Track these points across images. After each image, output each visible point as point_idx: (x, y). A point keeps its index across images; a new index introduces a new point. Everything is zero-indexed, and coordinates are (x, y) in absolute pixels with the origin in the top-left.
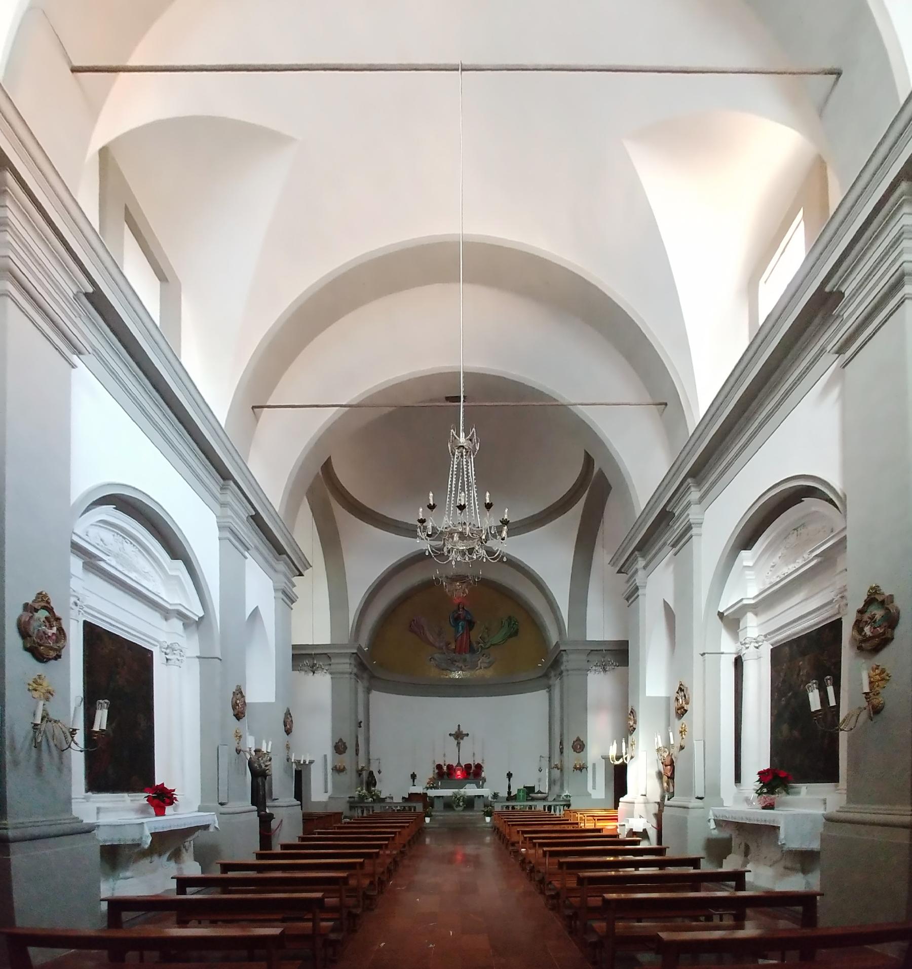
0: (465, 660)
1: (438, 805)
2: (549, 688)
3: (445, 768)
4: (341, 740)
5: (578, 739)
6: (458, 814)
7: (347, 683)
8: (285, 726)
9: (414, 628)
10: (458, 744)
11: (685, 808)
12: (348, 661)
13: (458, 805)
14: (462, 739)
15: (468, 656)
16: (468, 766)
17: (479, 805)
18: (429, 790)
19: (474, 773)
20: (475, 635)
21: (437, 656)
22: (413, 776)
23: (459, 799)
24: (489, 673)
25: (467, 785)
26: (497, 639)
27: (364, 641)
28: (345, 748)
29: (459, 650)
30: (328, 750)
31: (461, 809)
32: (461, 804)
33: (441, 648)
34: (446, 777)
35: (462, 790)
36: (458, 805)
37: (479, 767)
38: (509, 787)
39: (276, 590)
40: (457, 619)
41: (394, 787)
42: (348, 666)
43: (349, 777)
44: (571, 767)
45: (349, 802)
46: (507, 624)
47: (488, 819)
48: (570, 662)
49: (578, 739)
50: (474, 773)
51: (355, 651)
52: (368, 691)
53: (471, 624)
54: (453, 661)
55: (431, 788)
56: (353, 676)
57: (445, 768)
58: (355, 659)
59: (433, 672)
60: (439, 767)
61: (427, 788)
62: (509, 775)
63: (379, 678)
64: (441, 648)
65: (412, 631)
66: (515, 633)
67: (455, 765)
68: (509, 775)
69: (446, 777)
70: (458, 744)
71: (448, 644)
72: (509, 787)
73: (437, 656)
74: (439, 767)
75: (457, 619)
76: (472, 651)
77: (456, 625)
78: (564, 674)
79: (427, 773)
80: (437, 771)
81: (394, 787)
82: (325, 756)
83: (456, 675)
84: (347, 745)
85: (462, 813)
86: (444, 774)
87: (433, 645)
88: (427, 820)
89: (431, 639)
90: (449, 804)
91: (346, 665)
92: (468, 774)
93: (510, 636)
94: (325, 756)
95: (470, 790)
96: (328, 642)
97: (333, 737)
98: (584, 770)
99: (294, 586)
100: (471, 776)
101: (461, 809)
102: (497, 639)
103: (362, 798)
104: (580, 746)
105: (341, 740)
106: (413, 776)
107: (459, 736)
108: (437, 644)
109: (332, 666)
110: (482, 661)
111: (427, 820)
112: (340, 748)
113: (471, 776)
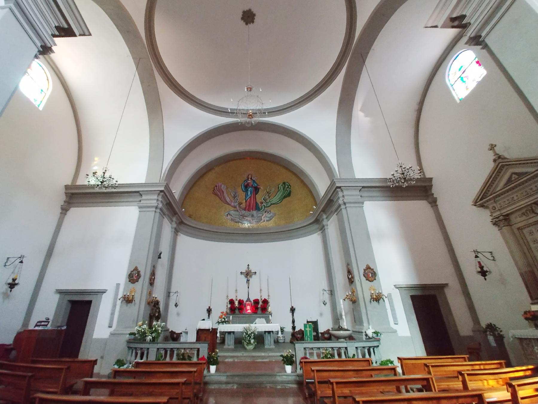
0: (253, 216)
1: (230, 342)
2: (322, 229)
3: (236, 303)
4: (136, 269)
5: (368, 268)
6: (249, 354)
7: (151, 216)
8: (150, 280)
9: (217, 192)
10: (248, 281)
11: (359, 332)
12: (155, 197)
13: (249, 343)
14: (251, 276)
15: (255, 213)
16: (256, 302)
17: (269, 341)
18: (221, 325)
19: (261, 308)
20: (260, 198)
21: (232, 212)
22: (209, 311)
23: (249, 336)
24: (271, 224)
25: (258, 320)
26: (275, 200)
27: (177, 190)
28: (139, 276)
29: (248, 208)
30: (122, 278)
31: (251, 347)
32: (252, 341)
33: (235, 207)
34: (237, 311)
35: (253, 326)
36: (249, 343)
37: (266, 302)
38: (293, 322)
39: (172, 228)
40: (246, 187)
41: (187, 320)
42: (155, 201)
43: (140, 308)
44: (368, 298)
45: (129, 342)
46: (282, 188)
47: (289, 369)
48: (347, 196)
49: (368, 268)
50: (261, 308)
51: (162, 189)
52: (176, 232)
53: (256, 190)
54: (244, 216)
55: (223, 322)
56: (158, 211)
57: (236, 303)
58: (163, 197)
59: (230, 224)
60: (232, 302)
61: (219, 323)
62: (293, 310)
63: (186, 224)
64: (235, 207)
65: (216, 195)
66: (289, 195)
67: (245, 300)
68: (293, 310)
69: (237, 311)
70: (248, 281)
71: (240, 204)
72: (293, 322)
73: (232, 212)
74: (232, 302)
75: (246, 187)
76: (257, 208)
77: (246, 191)
78: (343, 207)
79: (221, 307)
80: (229, 306)
81: (187, 320)
82: (118, 285)
83: (246, 225)
84: (142, 273)
85: (254, 354)
86: (236, 309)
87: (228, 204)
88: (213, 368)
89: (228, 200)
90: (240, 341)
91: (153, 200)
92: (257, 308)
93: (285, 197)
94: (118, 285)
95: (260, 325)
96: (144, 182)
97: (129, 266)
98: (381, 301)
99: (55, 45)
100: (259, 311)
101: (251, 347)
102: (275, 200)
103: (143, 334)
104: (371, 274)
105: (136, 269)
106: (209, 311)
107: (248, 274)
108: (233, 204)
109: (142, 202)
110: (265, 217)
111: (213, 368)
112: (134, 277)
113: (259, 311)
